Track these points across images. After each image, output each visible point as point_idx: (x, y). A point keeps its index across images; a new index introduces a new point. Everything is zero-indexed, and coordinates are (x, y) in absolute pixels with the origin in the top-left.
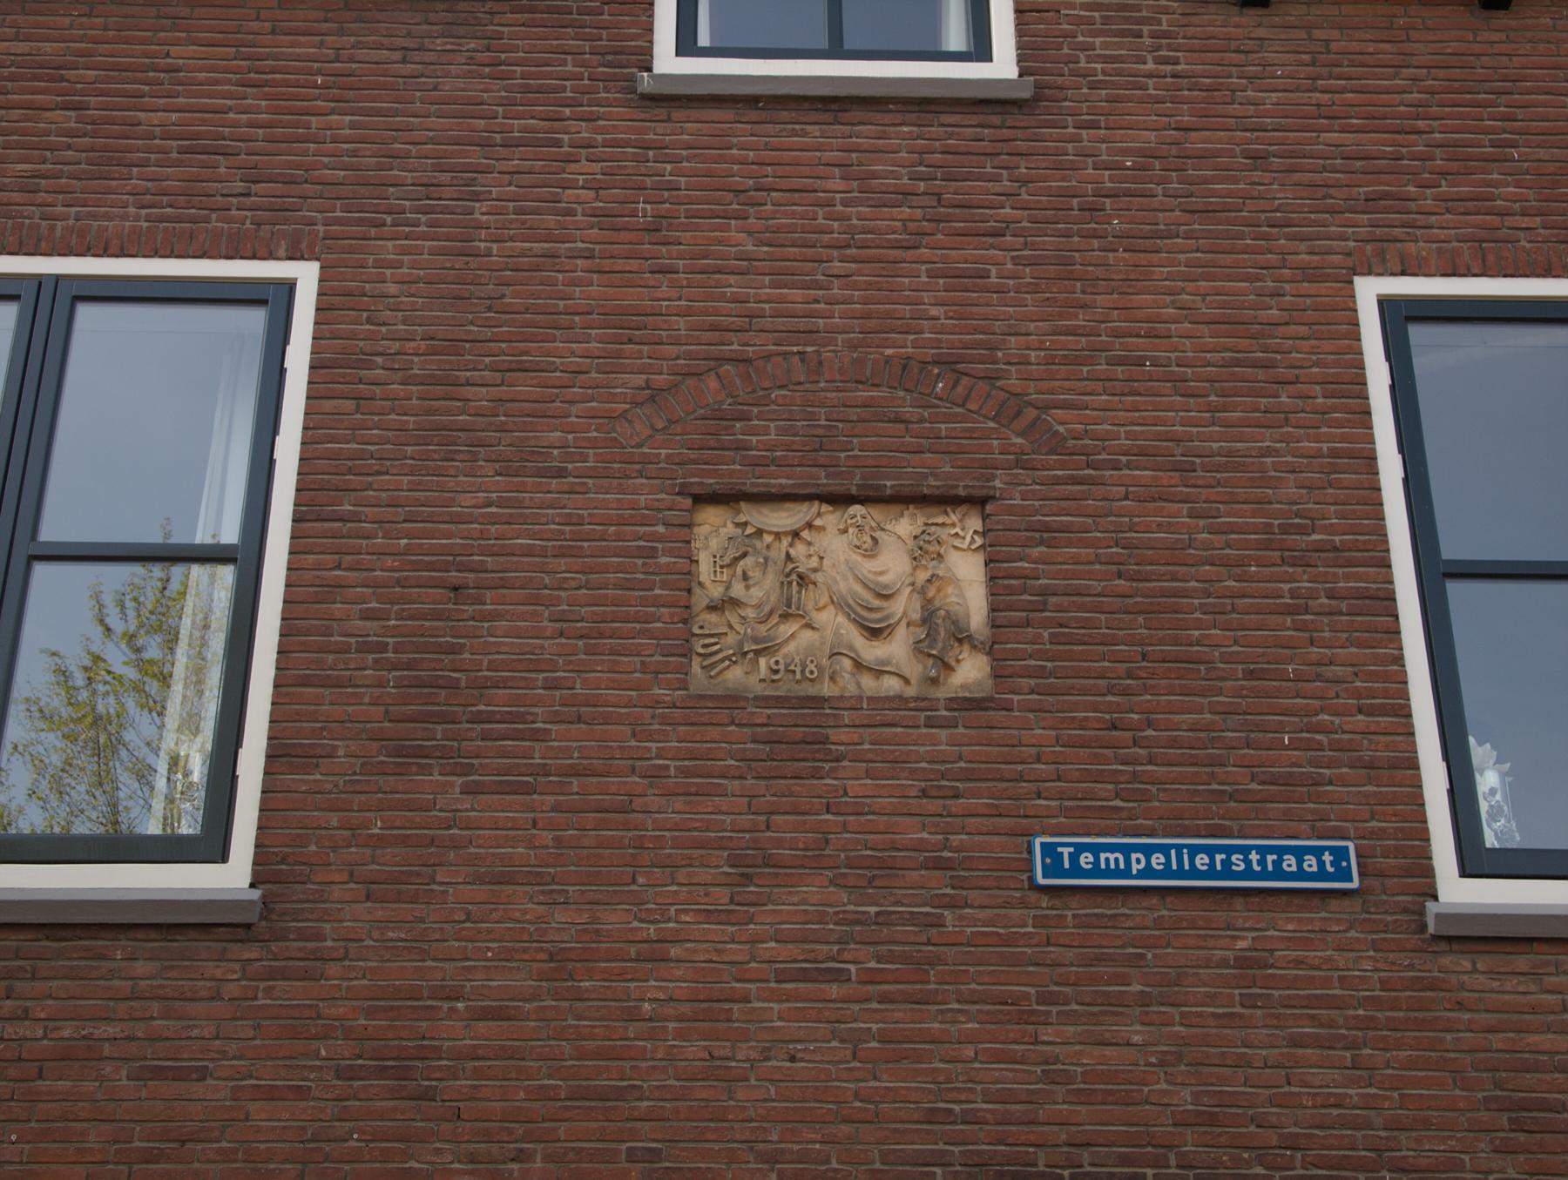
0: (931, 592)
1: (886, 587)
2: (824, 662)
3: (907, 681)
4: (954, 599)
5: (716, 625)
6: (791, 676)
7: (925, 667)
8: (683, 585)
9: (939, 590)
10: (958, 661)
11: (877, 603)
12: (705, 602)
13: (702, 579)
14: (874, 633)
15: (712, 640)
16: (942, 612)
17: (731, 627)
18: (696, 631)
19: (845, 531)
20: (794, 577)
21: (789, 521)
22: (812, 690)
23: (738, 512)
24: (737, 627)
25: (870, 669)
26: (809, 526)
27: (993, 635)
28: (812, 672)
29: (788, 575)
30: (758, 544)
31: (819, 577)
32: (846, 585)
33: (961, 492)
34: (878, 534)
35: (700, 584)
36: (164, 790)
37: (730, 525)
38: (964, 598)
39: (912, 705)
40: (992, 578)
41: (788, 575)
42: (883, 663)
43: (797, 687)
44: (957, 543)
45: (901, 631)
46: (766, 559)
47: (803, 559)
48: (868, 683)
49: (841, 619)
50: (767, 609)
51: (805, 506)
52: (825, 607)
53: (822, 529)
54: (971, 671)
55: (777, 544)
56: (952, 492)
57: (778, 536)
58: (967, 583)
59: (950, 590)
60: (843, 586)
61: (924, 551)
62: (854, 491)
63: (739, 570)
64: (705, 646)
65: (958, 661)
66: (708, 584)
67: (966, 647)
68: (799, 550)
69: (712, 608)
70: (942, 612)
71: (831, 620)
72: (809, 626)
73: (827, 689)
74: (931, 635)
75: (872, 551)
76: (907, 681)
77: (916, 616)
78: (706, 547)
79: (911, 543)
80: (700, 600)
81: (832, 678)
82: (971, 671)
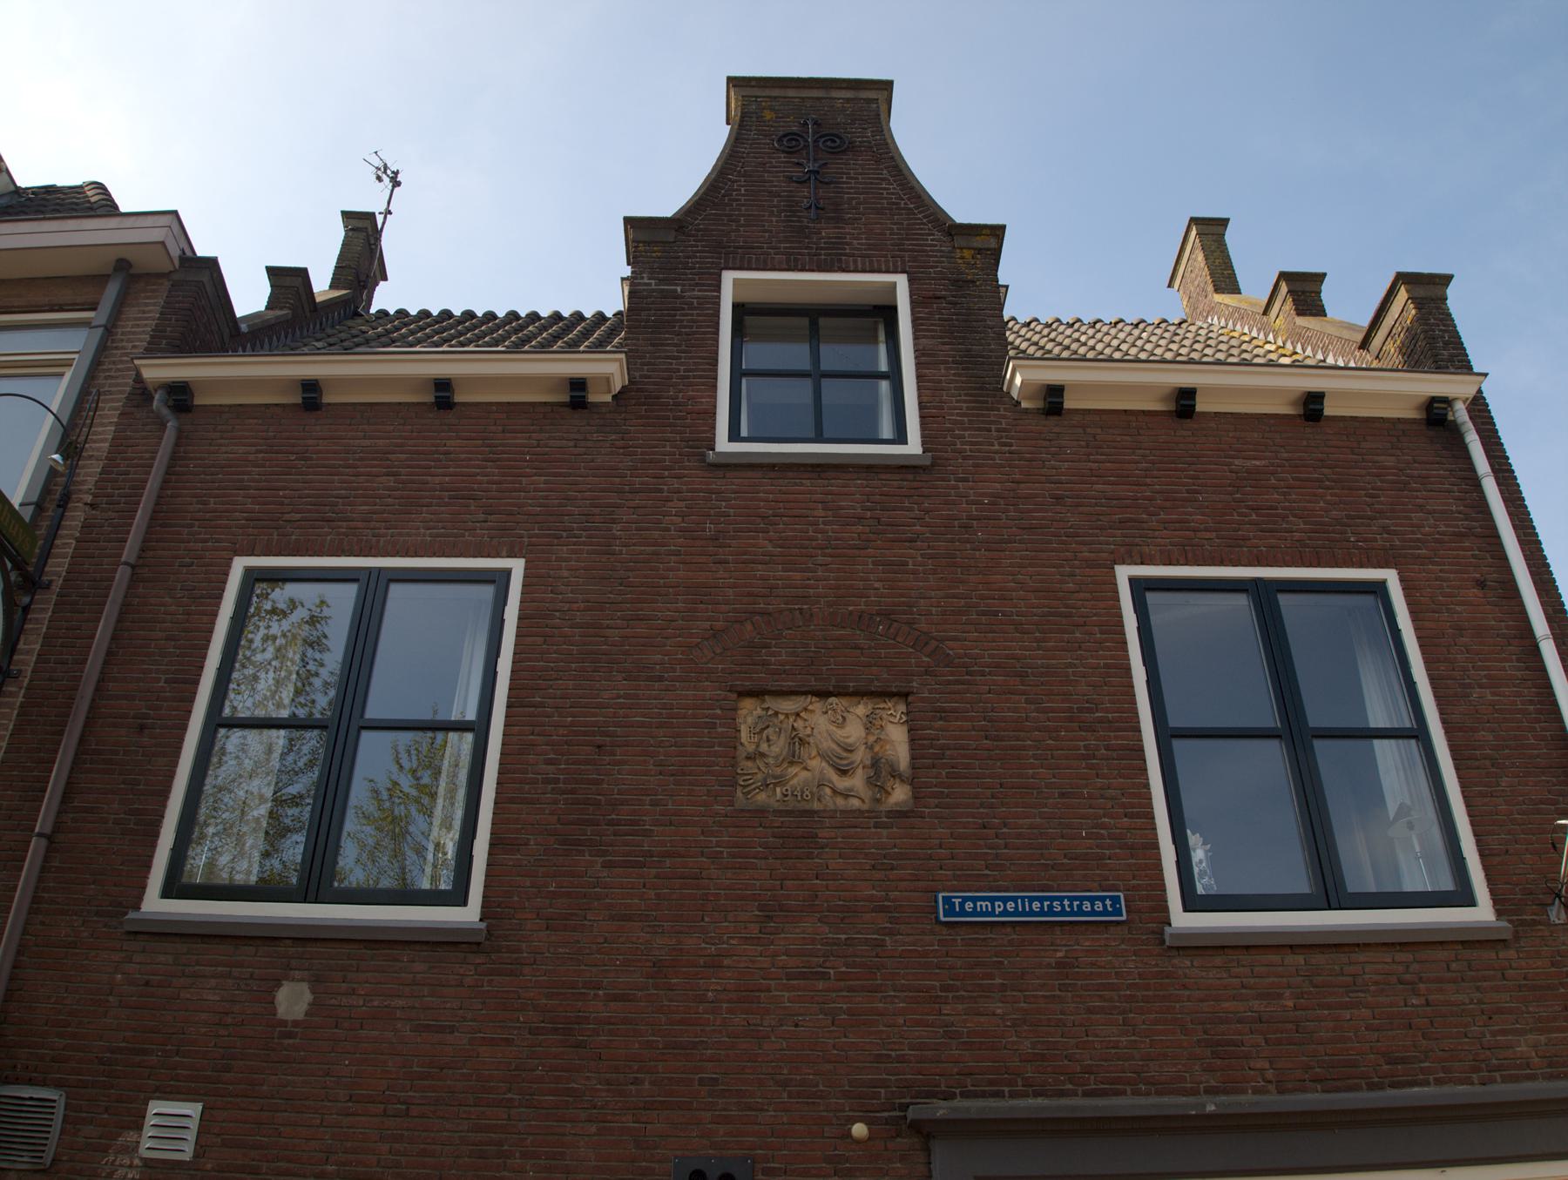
0: (877, 749)
14: (843, 773)
22: (807, 807)
31: (811, 740)
32: (827, 744)
45: (860, 771)
48: (840, 802)
54: (900, 794)
57: (787, 716)
61: (870, 723)
68: (799, 724)
69: (748, 758)
71: (815, 763)
72: (806, 769)
73: (816, 806)
74: (877, 774)
75: (841, 726)
77: (868, 762)
80: (741, 753)
82: (900, 794)
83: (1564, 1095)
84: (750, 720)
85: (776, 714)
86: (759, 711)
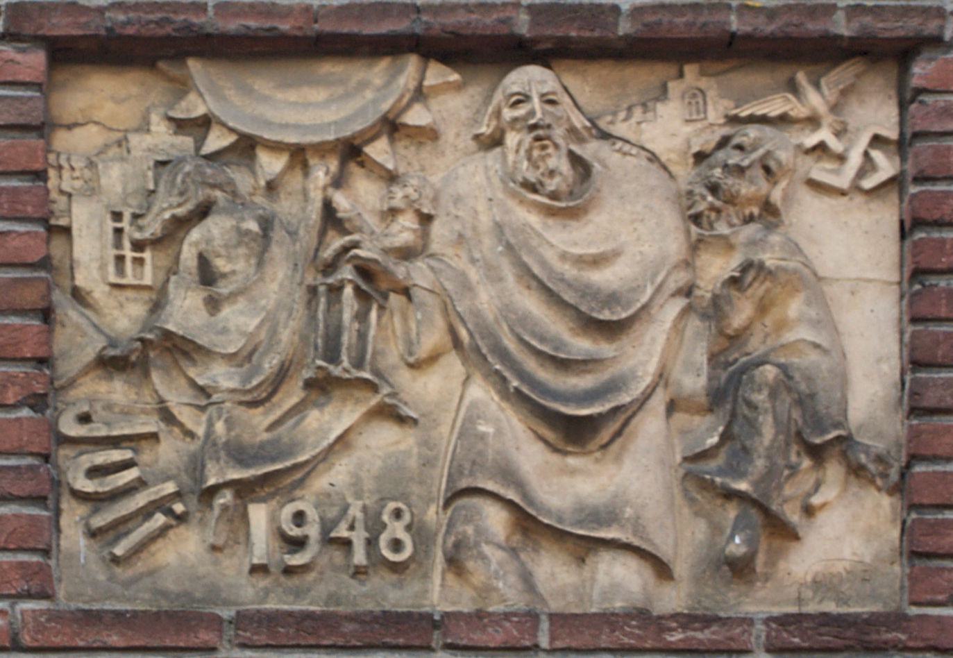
0: (741, 313)
1: (612, 299)
2: (432, 514)
3: (662, 569)
4: (804, 333)
5: (127, 413)
6: (338, 555)
7: (716, 528)
8: (31, 297)
9: (763, 308)
10: (809, 511)
11: (582, 345)
12: (92, 347)
13: (80, 281)
14: (574, 432)
15: (116, 455)
16: (769, 372)
17: (167, 416)
18: (70, 428)
19: (495, 141)
20: (347, 272)
21: (331, 115)
22: (396, 597)
23: (183, 87)
24: (186, 416)
25: (560, 536)
26: (391, 126)
27: (914, 434)
28: (397, 545)
29: (330, 267)
30: (242, 179)
31: (419, 274)
32: (495, 297)
33: (842, 27)
34: (590, 149)
35: (78, 295)
36: (540, 634)
37: (160, 128)
38: (835, 330)
39: (675, 637)
40: (918, 273)
41: (330, 267)
42: (607, 515)
43: (355, 589)
44: (821, 171)
45: (651, 426)
46: (266, 224)
47: (372, 221)
48: (554, 573)
49: (480, 392)
50: (270, 364)
51: (377, 71)
52: (433, 358)
53: (429, 135)
54: (844, 539)
55: (295, 181)
56: (814, 27)
57: (299, 155)
58: (846, 284)
59: (795, 307)
60: (486, 299)
61: (721, 195)
62: (523, 25)
63: (188, 255)
64: (95, 472)
65: (809, 511)
66: (99, 293)
67: (834, 471)
68: (361, 197)
69: (112, 364)
70: (769, 372)
71: (446, 391)
72: (390, 413)
73: (438, 593)
74: (735, 439)
75: (572, 198)
76: (662, 569)
77: (694, 382)
78: (92, 191)
79: (685, 173)
80: (77, 341)
81: (454, 563)
82: (844, 539)
83: (2, 363)
84: (114, 178)
85: (246, 147)
86: (161, 137)
